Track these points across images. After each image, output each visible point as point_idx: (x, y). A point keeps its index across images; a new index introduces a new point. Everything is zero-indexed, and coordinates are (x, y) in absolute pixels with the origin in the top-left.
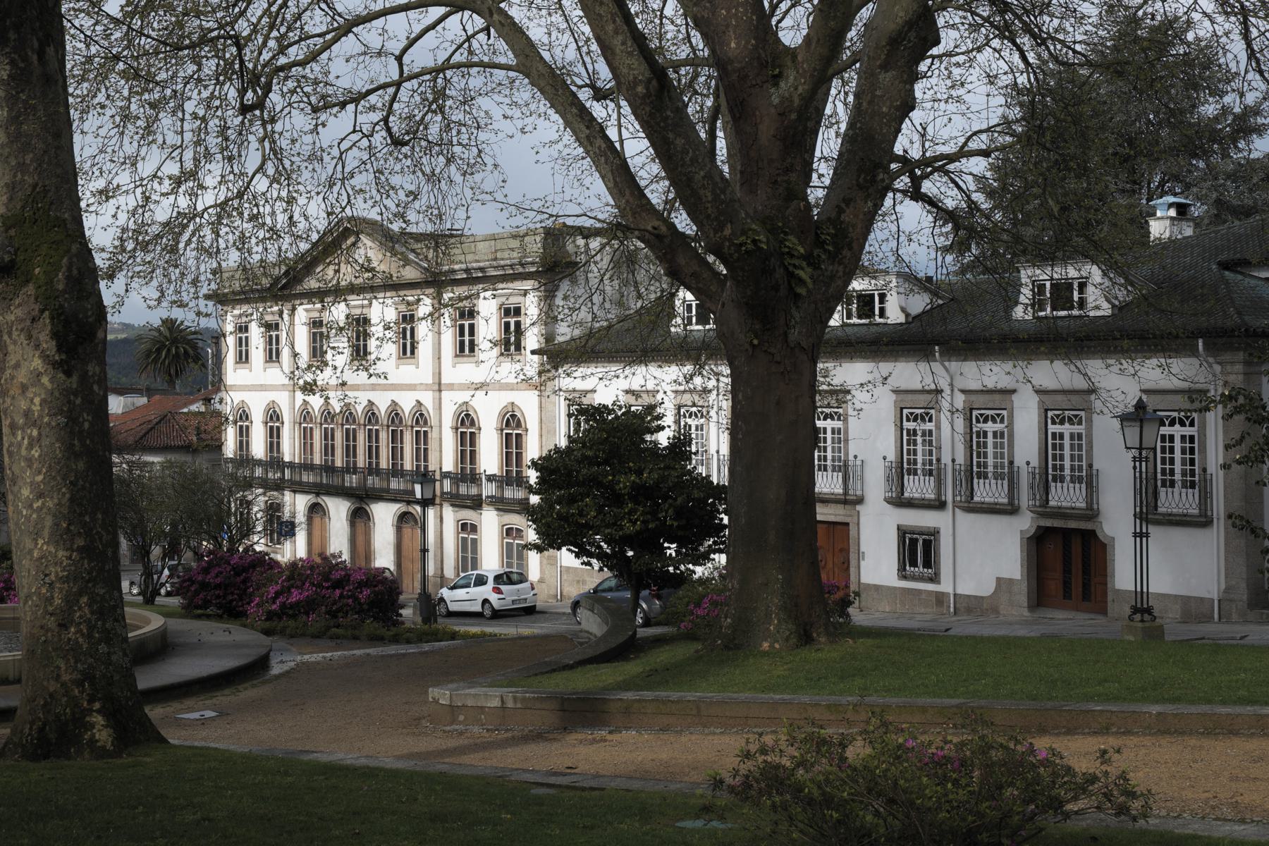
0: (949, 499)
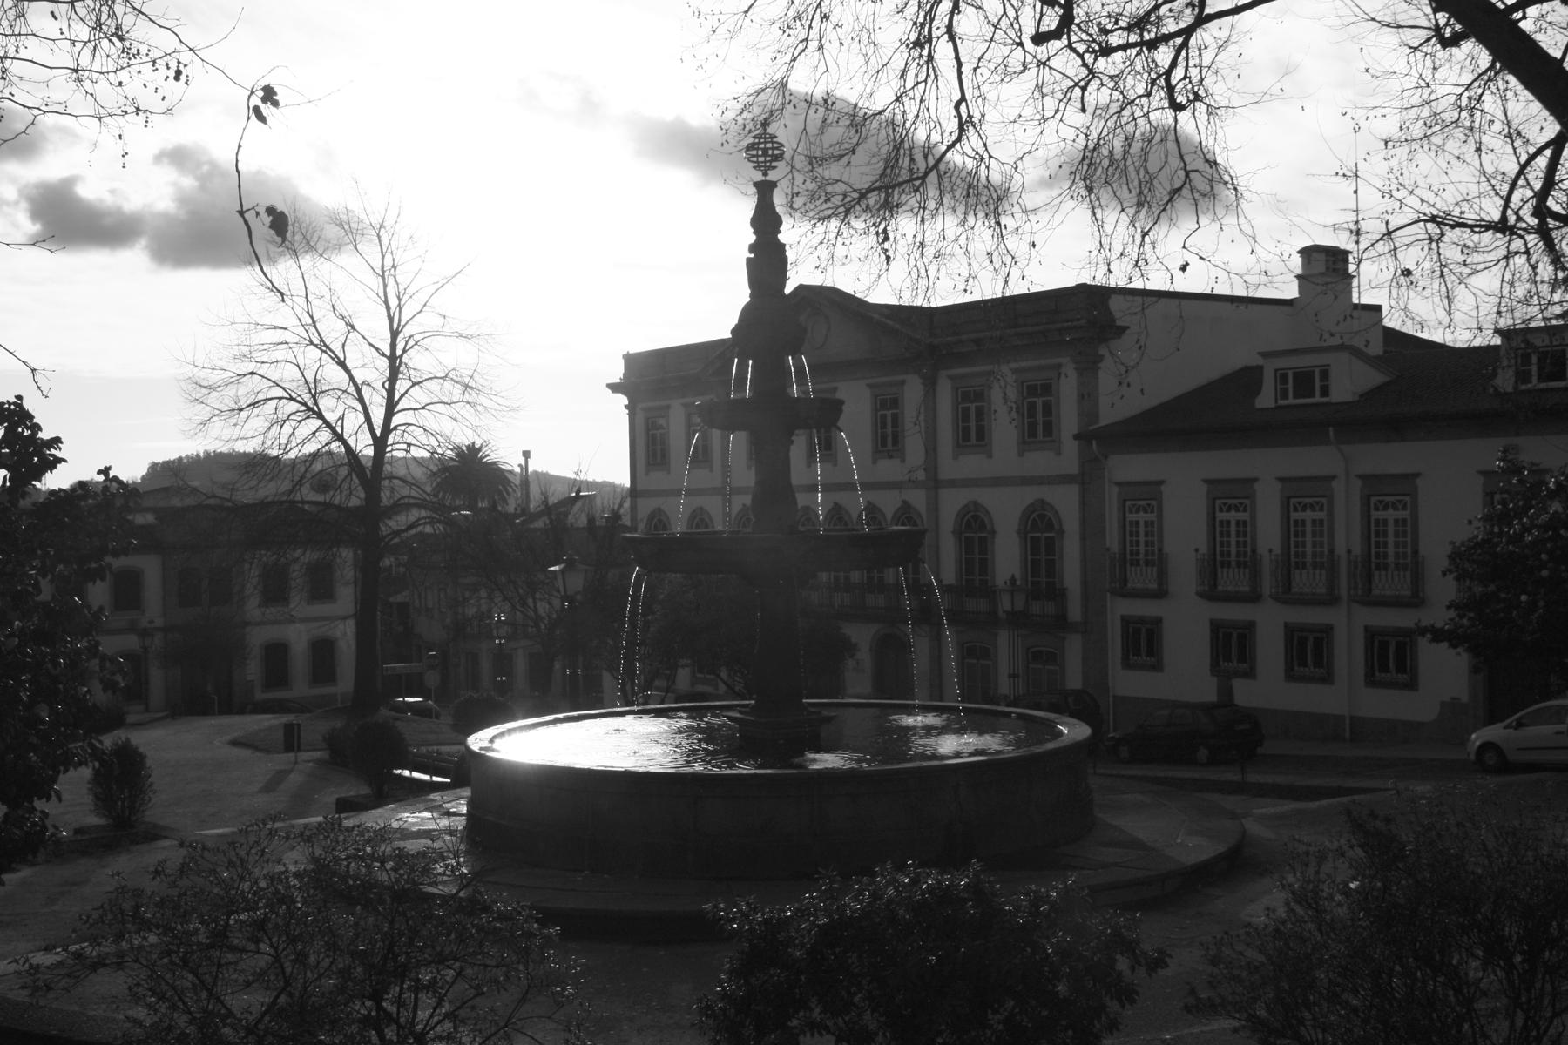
0: (1344, 592)
